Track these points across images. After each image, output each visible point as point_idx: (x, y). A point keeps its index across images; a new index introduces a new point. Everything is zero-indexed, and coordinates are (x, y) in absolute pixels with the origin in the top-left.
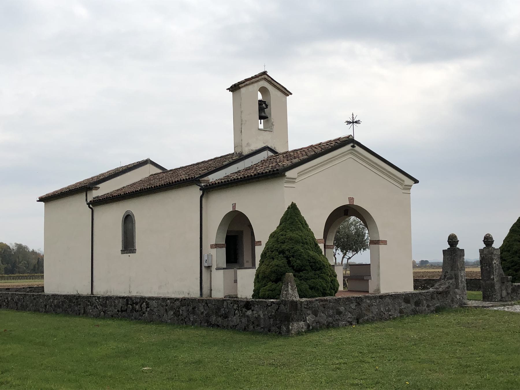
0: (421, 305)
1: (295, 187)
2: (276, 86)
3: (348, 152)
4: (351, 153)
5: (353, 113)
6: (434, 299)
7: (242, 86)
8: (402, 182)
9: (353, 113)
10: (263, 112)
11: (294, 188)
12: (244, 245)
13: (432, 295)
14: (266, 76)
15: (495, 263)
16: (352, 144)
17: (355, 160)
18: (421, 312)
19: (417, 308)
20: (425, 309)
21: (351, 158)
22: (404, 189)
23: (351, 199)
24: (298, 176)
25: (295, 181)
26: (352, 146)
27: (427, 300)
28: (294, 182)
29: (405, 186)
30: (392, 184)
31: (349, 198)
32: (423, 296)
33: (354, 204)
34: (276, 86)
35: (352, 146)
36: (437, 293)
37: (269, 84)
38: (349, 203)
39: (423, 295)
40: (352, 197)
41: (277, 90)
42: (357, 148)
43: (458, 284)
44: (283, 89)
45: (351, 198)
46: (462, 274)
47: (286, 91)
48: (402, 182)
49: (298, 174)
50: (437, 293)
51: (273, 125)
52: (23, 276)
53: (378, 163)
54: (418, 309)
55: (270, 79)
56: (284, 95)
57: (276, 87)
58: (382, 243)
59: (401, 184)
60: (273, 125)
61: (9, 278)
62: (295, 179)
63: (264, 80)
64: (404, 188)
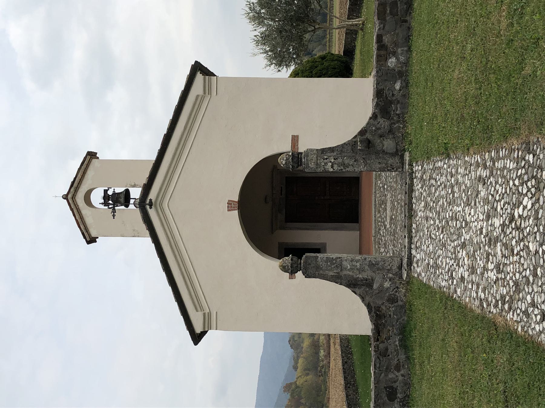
0: (395, 385)
1: (216, 312)
2: (80, 180)
3: (160, 211)
6: (387, 349)
7: (88, 236)
10: (119, 199)
12: (298, 242)
14: (70, 196)
15: (332, 167)
16: (148, 207)
18: (408, 385)
19: (399, 395)
20: (402, 375)
21: (169, 204)
22: (210, 93)
23: (230, 205)
24: (202, 309)
25: (208, 313)
26: (151, 208)
27: (388, 370)
28: (210, 314)
29: (205, 93)
35: (151, 208)
36: (378, 340)
37: (79, 190)
40: (228, 203)
41: (86, 176)
42: (152, 195)
44: (83, 167)
45: (228, 207)
46: (349, 267)
47: (85, 163)
49: (197, 311)
50: (378, 340)
53: (173, 152)
55: (72, 190)
58: (296, 147)
59: (203, 98)
60: (135, 185)
62: (204, 314)
64: (209, 94)
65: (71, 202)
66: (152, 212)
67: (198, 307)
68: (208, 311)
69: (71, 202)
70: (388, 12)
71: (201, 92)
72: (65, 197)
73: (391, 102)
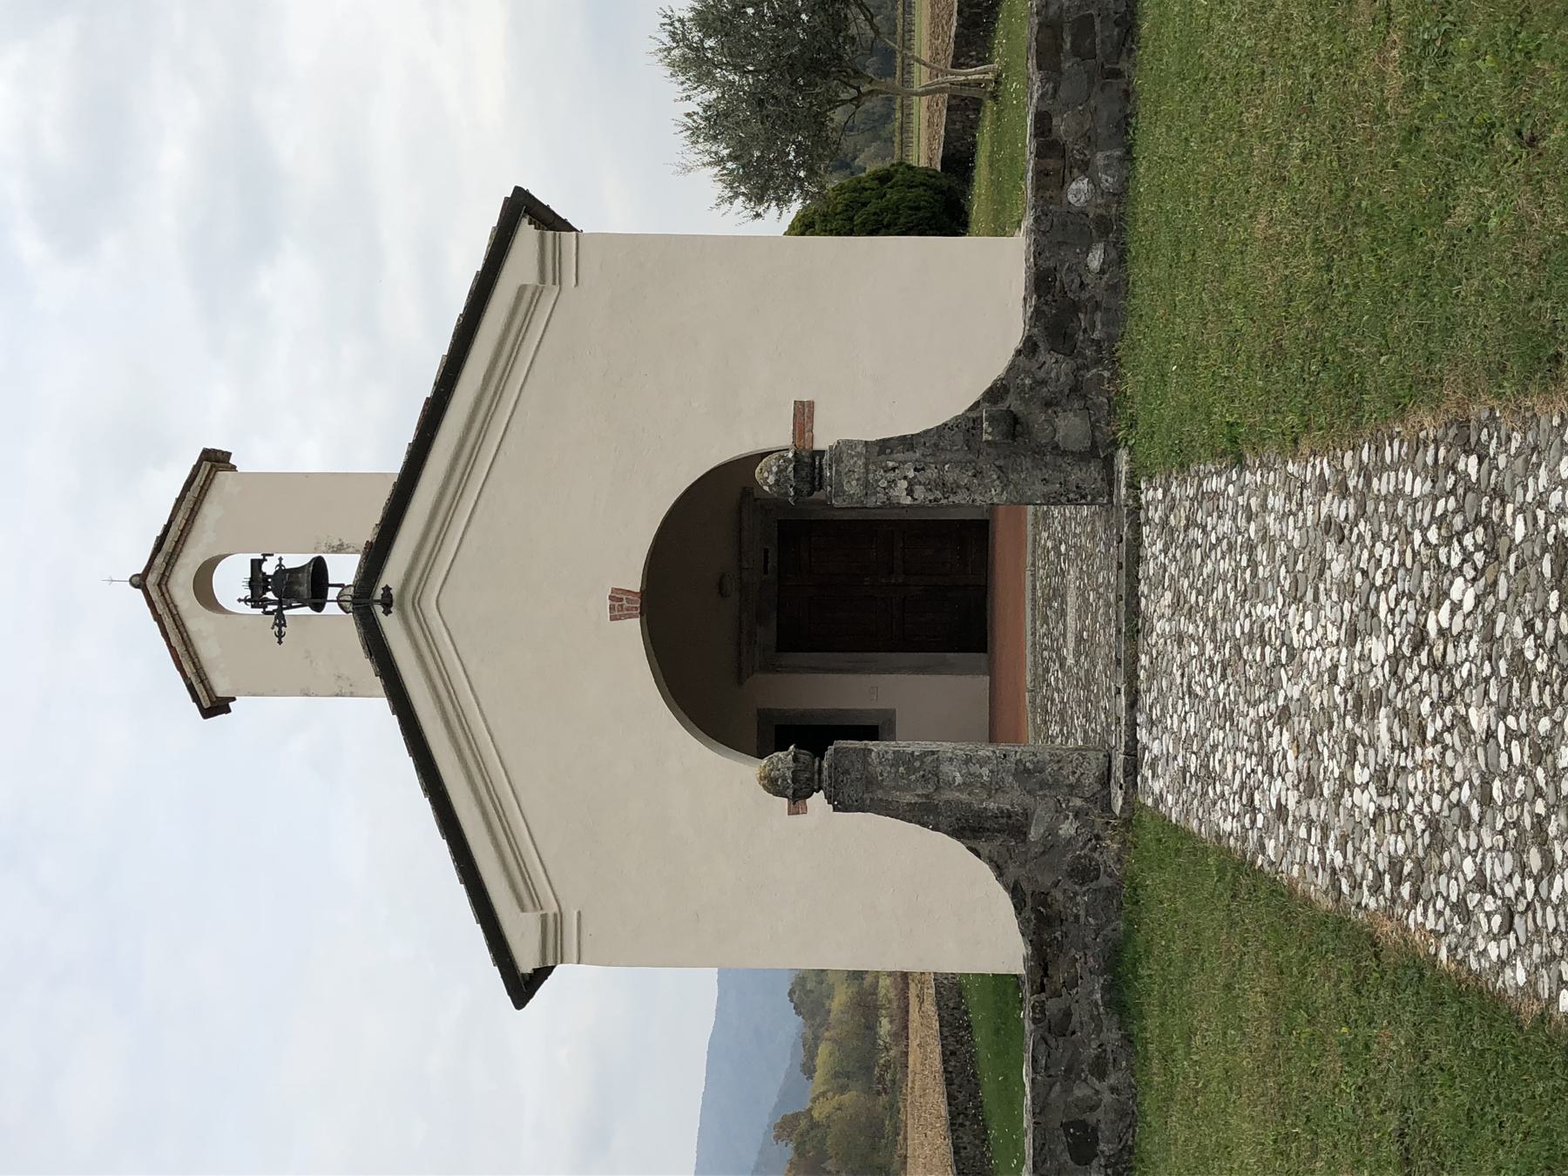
0: (1091, 1118)
1: (579, 913)
4: (417, 603)
5: (240, 600)
8: (528, 295)
9: (240, 600)
11: (582, 914)
13: (1050, 1031)
14: (152, 579)
15: (910, 492)
17: (449, 634)
18: (1128, 1116)
19: (1102, 1146)
20: (1113, 1089)
22: (558, 279)
23: (617, 604)
24: (537, 903)
25: (555, 915)
26: (387, 612)
28: (559, 918)
29: (542, 279)
30: (540, 352)
31: (613, 618)
32: (1053, 1095)
33: (637, 589)
34: (184, 528)
35: (387, 612)
38: (635, 616)
39: (1048, 1094)
41: (199, 521)
42: (392, 575)
43: (1003, 821)
45: (612, 608)
46: (959, 780)
47: (196, 483)
48: (528, 295)
49: (523, 909)
50: (1042, 989)
51: (342, 545)
52: (903, 69)
54: (1109, 1142)
55: (159, 560)
56: (213, 485)
57: (188, 527)
59: (538, 294)
61: (906, 111)
62: (544, 918)
63: (166, 584)
64: (554, 283)
65: (155, 596)
66: (391, 626)
67: (526, 896)
68: (556, 909)
69: (155, 596)
70: (1068, 46)
71: (532, 278)
72: (139, 582)
73: (1075, 307)
